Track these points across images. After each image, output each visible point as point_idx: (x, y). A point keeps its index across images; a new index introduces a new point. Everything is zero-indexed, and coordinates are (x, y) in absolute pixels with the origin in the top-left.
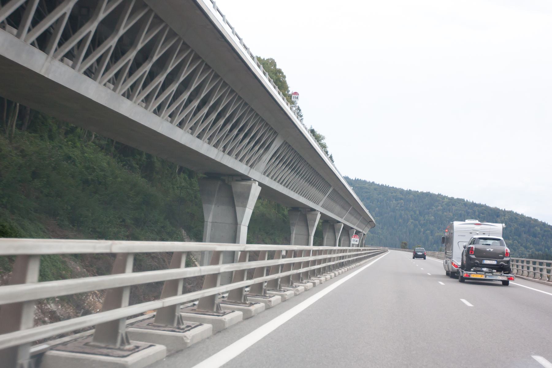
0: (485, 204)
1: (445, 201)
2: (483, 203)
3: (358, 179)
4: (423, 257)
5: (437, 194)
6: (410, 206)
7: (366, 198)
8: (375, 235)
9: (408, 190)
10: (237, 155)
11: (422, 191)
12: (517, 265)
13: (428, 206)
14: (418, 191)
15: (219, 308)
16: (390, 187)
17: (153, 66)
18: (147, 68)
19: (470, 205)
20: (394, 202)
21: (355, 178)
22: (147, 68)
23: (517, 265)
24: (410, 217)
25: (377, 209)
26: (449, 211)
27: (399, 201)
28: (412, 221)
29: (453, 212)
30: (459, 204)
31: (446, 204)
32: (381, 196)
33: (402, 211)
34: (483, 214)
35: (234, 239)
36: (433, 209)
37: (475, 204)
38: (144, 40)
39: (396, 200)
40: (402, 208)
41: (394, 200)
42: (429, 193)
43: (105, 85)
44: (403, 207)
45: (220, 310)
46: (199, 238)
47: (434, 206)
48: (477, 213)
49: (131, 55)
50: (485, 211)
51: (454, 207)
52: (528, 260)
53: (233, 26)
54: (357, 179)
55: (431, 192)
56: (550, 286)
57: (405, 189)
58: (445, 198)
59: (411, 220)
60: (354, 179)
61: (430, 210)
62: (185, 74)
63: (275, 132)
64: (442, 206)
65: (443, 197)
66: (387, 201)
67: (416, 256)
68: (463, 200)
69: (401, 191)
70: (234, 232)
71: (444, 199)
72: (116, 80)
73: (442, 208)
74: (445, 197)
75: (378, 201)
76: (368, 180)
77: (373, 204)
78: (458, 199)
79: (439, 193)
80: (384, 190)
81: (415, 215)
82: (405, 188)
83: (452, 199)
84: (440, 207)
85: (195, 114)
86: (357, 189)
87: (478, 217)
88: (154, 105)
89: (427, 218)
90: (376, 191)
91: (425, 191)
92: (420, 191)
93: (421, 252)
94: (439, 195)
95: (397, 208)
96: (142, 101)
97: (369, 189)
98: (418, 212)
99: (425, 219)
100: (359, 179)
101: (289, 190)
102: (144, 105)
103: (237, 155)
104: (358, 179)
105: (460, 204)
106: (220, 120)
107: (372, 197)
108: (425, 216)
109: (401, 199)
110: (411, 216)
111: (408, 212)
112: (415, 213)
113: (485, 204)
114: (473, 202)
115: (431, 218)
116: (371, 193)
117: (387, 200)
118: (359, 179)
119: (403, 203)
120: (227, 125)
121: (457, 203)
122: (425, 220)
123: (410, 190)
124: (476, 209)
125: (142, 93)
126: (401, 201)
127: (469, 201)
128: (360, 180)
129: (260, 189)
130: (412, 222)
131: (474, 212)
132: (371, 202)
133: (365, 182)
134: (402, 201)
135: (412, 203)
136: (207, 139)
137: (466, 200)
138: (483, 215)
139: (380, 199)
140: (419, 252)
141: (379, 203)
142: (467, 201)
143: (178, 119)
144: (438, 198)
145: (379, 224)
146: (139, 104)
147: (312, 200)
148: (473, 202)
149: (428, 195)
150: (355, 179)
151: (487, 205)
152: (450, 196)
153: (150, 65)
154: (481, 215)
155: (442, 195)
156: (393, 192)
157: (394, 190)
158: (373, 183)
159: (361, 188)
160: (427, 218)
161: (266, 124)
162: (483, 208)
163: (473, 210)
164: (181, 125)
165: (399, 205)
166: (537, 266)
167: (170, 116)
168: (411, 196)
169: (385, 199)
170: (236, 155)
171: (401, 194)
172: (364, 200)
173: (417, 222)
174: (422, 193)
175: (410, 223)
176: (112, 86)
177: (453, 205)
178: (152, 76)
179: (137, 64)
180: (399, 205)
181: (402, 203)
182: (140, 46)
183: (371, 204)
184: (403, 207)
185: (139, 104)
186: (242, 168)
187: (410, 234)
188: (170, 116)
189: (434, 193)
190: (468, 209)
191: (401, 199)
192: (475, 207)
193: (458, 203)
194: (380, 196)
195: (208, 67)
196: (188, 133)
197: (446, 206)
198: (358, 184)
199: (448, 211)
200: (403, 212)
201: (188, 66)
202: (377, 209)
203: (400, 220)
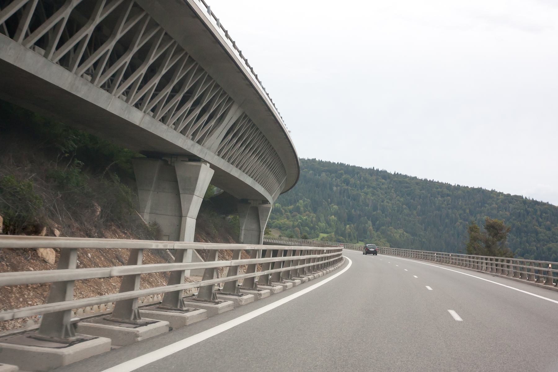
0: (548, 202)
1: (501, 199)
2: (545, 201)
3: (398, 173)
4: (375, 253)
5: (490, 190)
6: (458, 203)
7: (407, 194)
8: (415, 238)
9: (456, 186)
10: (194, 135)
11: (472, 187)
12: (496, 264)
13: (480, 204)
14: (467, 187)
15: (182, 304)
16: (435, 182)
17: (133, 58)
18: (127, 59)
19: (530, 203)
20: (440, 198)
21: (394, 172)
22: (127, 59)
23: (496, 264)
24: (459, 216)
25: (419, 207)
26: (506, 210)
27: (446, 198)
28: (461, 221)
29: (510, 211)
30: (517, 201)
31: (502, 202)
32: (424, 192)
33: (449, 209)
34: (546, 213)
35: (178, 236)
36: (486, 207)
37: (536, 201)
38: (122, 31)
39: (442, 197)
40: (449, 205)
41: (440, 196)
42: (481, 188)
43: (82, 76)
44: (450, 204)
45: (184, 307)
46: (238, 242)
47: (488, 204)
48: (539, 213)
49: (109, 46)
50: (549, 211)
51: (510, 205)
52: (393, 248)
53: (217, 17)
54: (396, 173)
55: (483, 188)
56: (542, 288)
57: (453, 185)
58: (501, 195)
59: (460, 221)
60: (393, 173)
61: (482, 208)
62: (168, 66)
63: (230, 99)
64: (496, 204)
65: (498, 194)
66: (432, 198)
67: (367, 252)
68: (521, 197)
69: (448, 186)
70: (178, 226)
71: (499, 196)
72: (92, 73)
73: (497, 206)
74: (500, 193)
75: (420, 198)
76: (409, 174)
77: (414, 201)
78: (516, 196)
79: (493, 190)
80: (428, 184)
81: (465, 214)
82: (453, 183)
83: (509, 195)
84: (494, 205)
85: (178, 109)
86: (395, 183)
87: (540, 217)
88: (136, 97)
89: (478, 218)
90: (418, 185)
91: (476, 187)
92: (470, 187)
93: (373, 248)
94: (493, 191)
95: (444, 206)
96: (123, 94)
97: (410, 184)
98: (468, 211)
99: (476, 219)
100: (399, 174)
101: (235, 168)
102: (125, 98)
103: (194, 135)
104: (398, 173)
105: (518, 202)
106: (204, 116)
107: (413, 193)
108: (477, 215)
109: (448, 195)
110: (460, 215)
111: (456, 211)
112: (464, 211)
113: (548, 202)
114: (533, 199)
115: (484, 218)
116: (412, 188)
117: (431, 197)
118: (399, 174)
119: (451, 200)
120: (211, 121)
121: (515, 201)
122: (477, 220)
123: (458, 185)
124: (537, 207)
125: (123, 85)
126: (448, 197)
127: (528, 198)
128: (400, 174)
129: (212, 172)
130: (461, 223)
131: (536, 211)
132: (411, 199)
133: (406, 176)
134: (449, 198)
135: (460, 199)
136: (191, 135)
137: (524, 198)
138: (546, 215)
139: (422, 195)
140: (371, 248)
141: (421, 200)
142: (526, 198)
143: (161, 114)
144: (492, 195)
145: (422, 225)
146: (119, 97)
147: (253, 176)
148: (533, 199)
149: (480, 190)
150: (395, 173)
151: (550, 203)
152: (505, 193)
153: (131, 56)
154: (544, 214)
155: (497, 192)
156: (438, 186)
157: (441, 185)
158: (416, 177)
159: (400, 182)
160: (478, 218)
161: (249, 120)
162: (546, 206)
163: (534, 209)
164: (163, 120)
165: (445, 203)
166: (489, 261)
167: (153, 110)
168: (460, 192)
169: (429, 195)
170: (218, 152)
171: (448, 189)
172: (404, 196)
173: (467, 222)
174: (473, 189)
175: (458, 223)
176: (89, 78)
177: (510, 202)
178: (133, 67)
179: (116, 55)
180: (445, 203)
181: (449, 200)
182: (119, 36)
183: (412, 201)
184: (450, 204)
185: (119, 97)
186: (196, 150)
187: (458, 237)
188: (153, 110)
189: (486, 189)
190: (528, 208)
191: (448, 195)
192: (537, 205)
193: (516, 200)
194: (422, 192)
195: (191, 60)
196: (172, 128)
197: (501, 204)
198: (397, 178)
199: (504, 210)
200: (450, 211)
201: (171, 58)
202: (419, 207)
203: (447, 220)
